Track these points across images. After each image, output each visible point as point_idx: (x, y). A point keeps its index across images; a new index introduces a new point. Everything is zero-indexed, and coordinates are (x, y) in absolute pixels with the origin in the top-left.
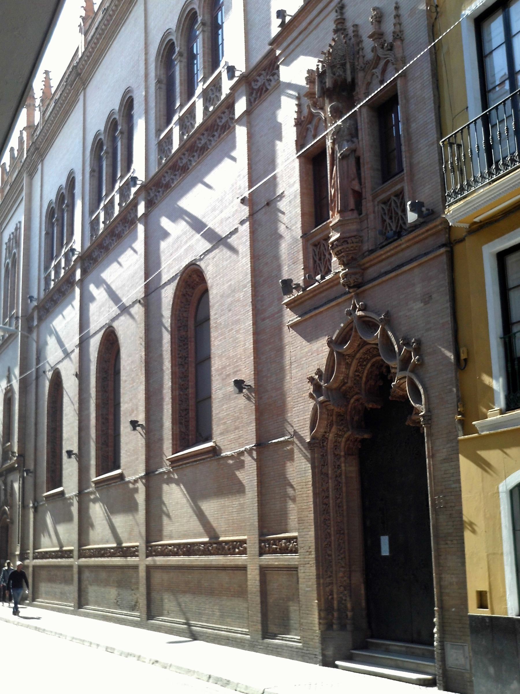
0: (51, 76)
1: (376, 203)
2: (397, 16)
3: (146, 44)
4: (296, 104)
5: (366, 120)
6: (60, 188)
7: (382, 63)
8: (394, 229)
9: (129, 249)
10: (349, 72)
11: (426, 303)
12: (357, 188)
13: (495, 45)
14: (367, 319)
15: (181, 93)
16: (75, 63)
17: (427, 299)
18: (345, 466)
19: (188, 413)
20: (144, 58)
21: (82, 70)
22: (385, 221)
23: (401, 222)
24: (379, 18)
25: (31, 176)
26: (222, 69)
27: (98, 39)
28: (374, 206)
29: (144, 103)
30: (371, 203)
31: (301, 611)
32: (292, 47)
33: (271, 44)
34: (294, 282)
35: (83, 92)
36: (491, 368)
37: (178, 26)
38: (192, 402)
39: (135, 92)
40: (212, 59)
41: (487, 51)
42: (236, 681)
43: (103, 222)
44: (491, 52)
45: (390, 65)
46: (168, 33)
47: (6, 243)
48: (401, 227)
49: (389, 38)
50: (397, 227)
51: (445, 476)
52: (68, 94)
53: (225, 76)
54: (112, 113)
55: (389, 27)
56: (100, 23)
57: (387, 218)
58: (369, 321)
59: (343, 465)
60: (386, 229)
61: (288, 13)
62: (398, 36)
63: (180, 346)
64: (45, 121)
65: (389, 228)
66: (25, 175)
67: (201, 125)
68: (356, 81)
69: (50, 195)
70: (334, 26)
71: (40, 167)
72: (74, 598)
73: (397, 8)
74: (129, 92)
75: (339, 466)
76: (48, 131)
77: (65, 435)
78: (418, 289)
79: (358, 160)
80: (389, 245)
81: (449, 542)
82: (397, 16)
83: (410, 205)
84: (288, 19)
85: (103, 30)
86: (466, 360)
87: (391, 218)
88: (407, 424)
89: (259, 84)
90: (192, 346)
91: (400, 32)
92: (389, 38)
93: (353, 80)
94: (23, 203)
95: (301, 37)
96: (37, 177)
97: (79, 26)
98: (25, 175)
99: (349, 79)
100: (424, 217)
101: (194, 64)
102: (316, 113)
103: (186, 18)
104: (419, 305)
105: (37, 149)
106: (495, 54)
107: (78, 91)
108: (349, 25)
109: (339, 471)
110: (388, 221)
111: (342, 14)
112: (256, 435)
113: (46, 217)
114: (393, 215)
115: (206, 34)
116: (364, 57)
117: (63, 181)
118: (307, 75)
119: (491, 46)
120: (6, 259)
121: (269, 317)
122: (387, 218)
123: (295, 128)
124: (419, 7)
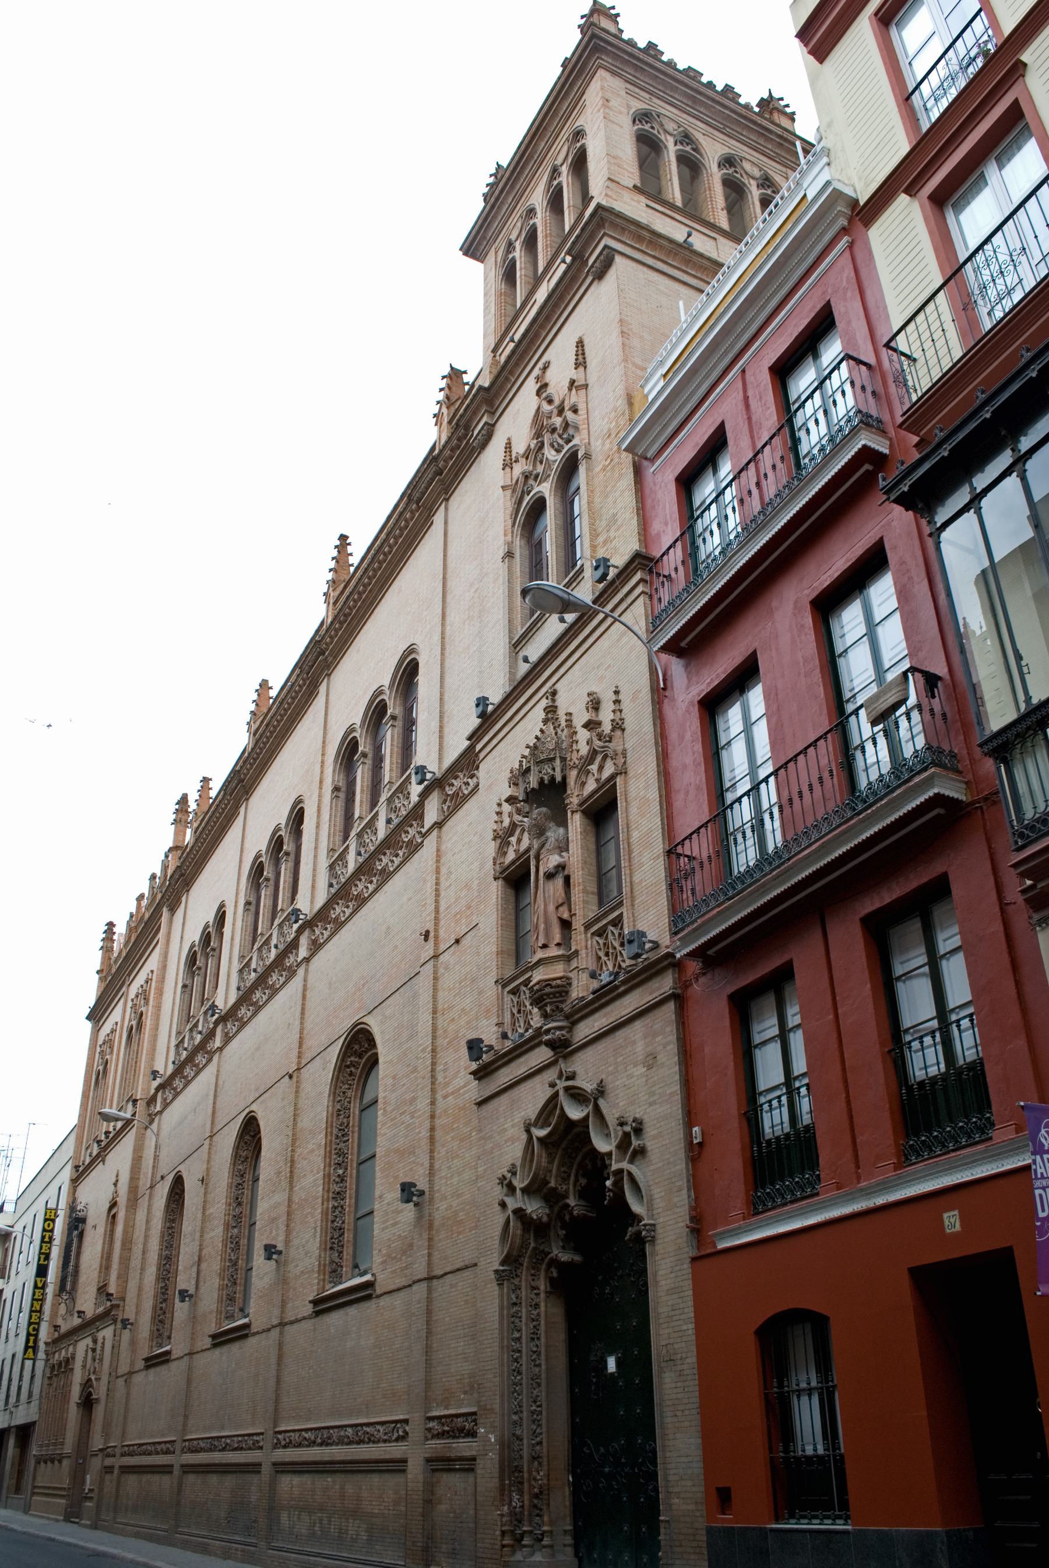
0: (211, 784)
1: (589, 935)
2: (617, 702)
3: (324, 742)
4: (455, 375)
5: (660, 494)
6: (206, 926)
7: (599, 758)
8: (611, 969)
9: (970, 998)
10: (558, 769)
11: (650, 1067)
12: (566, 916)
13: (850, 639)
14: (576, 1091)
15: (361, 802)
16: (238, 768)
17: (651, 1061)
18: (546, 1306)
19: (343, 1234)
20: (320, 760)
21: (245, 775)
22: (600, 958)
23: (619, 958)
24: (595, 704)
25: (173, 910)
26: (411, 770)
27: (268, 738)
28: (587, 941)
29: (316, 815)
30: (583, 936)
31: (479, 1536)
32: (495, 742)
33: (469, 739)
34: (486, 1043)
35: (326, 680)
36: (787, 962)
37: (363, 721)
38: (349, 1219)
39: (306, 802)
40: (403, 760)
41: (839, 648)
42: (592, 379)
43: (132, 1000)
44: (729, 743)
45: (609, 760)
46: (351, 729)
47: (132, 1000)
48: (620, 966)
49: (607, 727)
50: (615, 965)
51: (673, 1313)
52: (226, 805)
53: (414, 779)
54: (277, 829)
55: (606, 716)
56: (272, 718)
57: (601, 954)
58: (579, 1094)
59: (542, 1304)
60: (601, 969)
61: (491, 700)
62: (618, 726)
63: (337, 1137)
64: (198, 838)
65: (604, 968)
66: (165, 909)
67: (589, 1140)
68: (568, 781)
69: (194, 935)
70: (543, 715)
71: (184, 899)
72: (241, 1348)
73: (617, 693)
74: (301, 801)
75: (537, 1306)
76: (197, 852)
77: (1021, 792)
78: (640, 1048)
79: (567, 880)
80: (357, 1458)
81: (679, 1413)
82: (617, 702)
83: (867, 471)
84: (490, 708)
85: (275, 727)
86: (700, 1144)
87: (607, 954)
88: (564, 1232)
89: (454, 789)
90: (353, 1138)
91: (621, 719)
92: (607, 727)
93: (564, 778)
94: (135, 1128)
95: (940, 587)
96: (180, 913)
97: (325, 594)
98: (165, 909)
99: (559, 778)
100: (773, 109)
101: (412, 731)
102: (928, 783)
103: (374, 711)
104: (641, 1070)
105: (182, 875)
106: (851, 654)
107: (240, 800)
108: (561, 713)
109: (535, 1312)
110: (604, 958)
111: (554, 701)
112: (700, 1385)
113: (186, 964)
114: (611, 951)
115: (396, 730)
116: (578, 751)
117: (210, 917)
118: (704, 80)
119: (844, 643)
120: (130, 1020)
121: (453, 1093)
122: (601, 954)
123: (578, 36)
124: (906, 756)
